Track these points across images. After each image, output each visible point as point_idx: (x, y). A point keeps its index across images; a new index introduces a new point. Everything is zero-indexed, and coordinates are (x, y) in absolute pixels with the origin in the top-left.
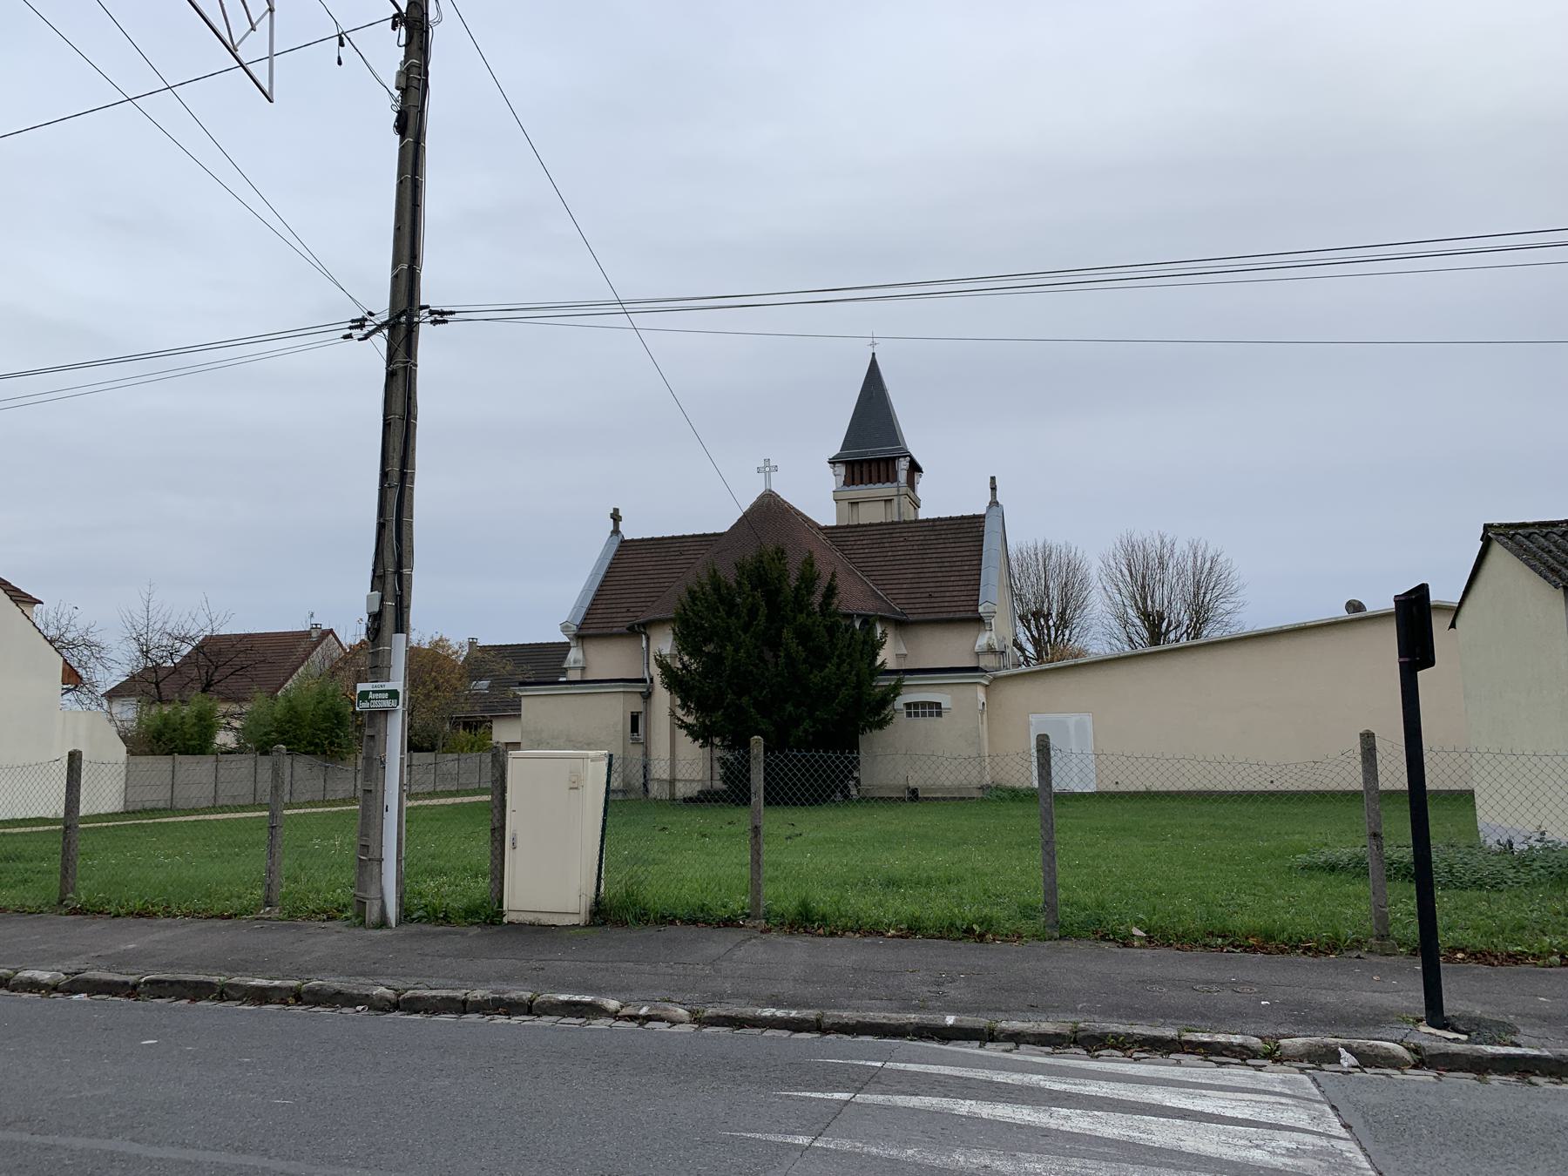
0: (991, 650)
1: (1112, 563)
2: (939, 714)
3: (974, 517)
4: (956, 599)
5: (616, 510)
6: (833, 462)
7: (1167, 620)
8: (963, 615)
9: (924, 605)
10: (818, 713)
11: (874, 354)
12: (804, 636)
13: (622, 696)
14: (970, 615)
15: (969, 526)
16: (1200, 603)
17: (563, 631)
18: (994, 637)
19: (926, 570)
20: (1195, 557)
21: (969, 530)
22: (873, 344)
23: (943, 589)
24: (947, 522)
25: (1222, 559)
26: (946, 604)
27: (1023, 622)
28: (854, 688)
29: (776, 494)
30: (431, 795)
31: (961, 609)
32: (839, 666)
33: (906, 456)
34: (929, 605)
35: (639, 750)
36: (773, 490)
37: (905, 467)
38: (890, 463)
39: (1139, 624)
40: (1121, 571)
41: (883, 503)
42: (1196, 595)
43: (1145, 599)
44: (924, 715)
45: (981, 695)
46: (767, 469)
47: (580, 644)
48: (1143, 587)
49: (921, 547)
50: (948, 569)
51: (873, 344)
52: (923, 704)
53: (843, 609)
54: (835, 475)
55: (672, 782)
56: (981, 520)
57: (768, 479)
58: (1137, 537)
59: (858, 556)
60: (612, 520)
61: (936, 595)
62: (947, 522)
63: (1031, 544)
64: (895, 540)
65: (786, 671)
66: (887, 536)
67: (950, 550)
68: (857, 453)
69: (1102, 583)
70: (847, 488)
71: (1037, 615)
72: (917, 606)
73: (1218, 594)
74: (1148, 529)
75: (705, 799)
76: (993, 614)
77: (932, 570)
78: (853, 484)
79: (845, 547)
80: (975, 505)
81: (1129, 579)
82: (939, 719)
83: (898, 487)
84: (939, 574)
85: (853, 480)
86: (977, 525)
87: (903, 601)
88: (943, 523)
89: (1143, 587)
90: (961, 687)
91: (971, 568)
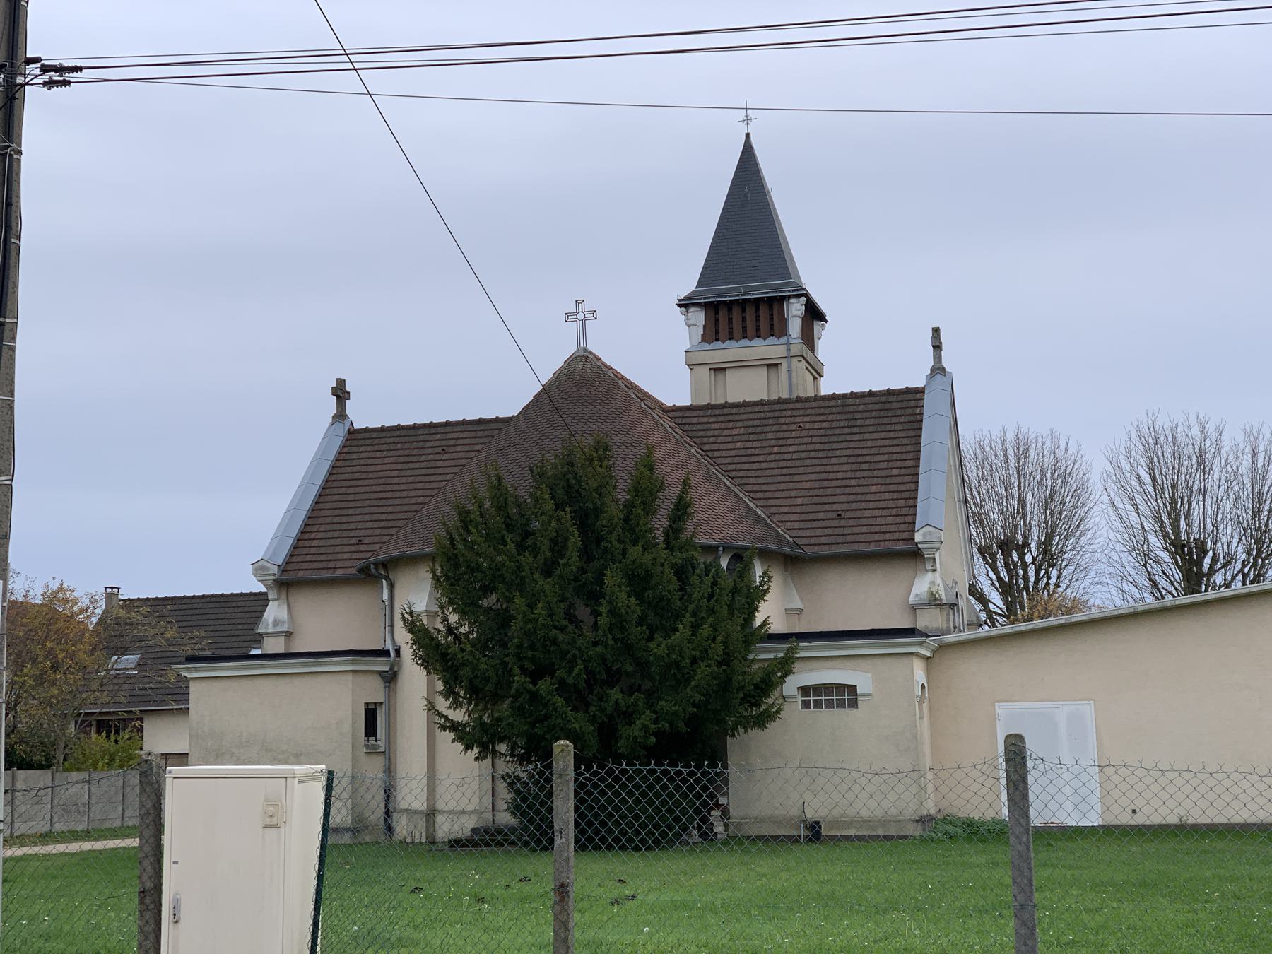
0: (934, 602)
2: (854, 704)
3: (908, 391)
4: (879, 521)
5: (341, 383)
6: (684, 304)
7: (1211, 553)
8: (890, 546)
11: (748, 135)
12: (639, 581)
13: (350, 677)
14: (900, 546)
17: (255, 575)
18: (939, 581)
19: (832, 476)
20: (1255, 455)
22: (747, 120)
24: (867, 400)
29: (595, 356)
31: (888, 536)
32: (695, 628)
36: (590, 348)
40: (1138, 477)
41: (766, 366)
44: (830, 705)
45: (919, 673)
46: (581, 316)
47: (284, 596)
48: (1173, 502)
50: (866, 474)
51: (747, 120)
52: (829, 688)
53: (702, 539)
55: (431, 814)
56: (918, 396)
57: (581, 333)
58: (1163, 423)
61: (849, 514)
63: (996, 434)
64: (784, 427)
65: (609, 636)
66: (771, 421)
67: (869, 443)
68: (723, 291)
69: (1109, 496)
71: (1006, 545)
72: (819, 532)
76: (937, 545)
79: (705, 440)
81: (1151, 489)
83: (788, 344)
84: (853, 482)
85: (717, 333)
86: (912, 404)
87: (796, 525)
88: (858, 401)
89: (1173, 502)
91: (903, 471)
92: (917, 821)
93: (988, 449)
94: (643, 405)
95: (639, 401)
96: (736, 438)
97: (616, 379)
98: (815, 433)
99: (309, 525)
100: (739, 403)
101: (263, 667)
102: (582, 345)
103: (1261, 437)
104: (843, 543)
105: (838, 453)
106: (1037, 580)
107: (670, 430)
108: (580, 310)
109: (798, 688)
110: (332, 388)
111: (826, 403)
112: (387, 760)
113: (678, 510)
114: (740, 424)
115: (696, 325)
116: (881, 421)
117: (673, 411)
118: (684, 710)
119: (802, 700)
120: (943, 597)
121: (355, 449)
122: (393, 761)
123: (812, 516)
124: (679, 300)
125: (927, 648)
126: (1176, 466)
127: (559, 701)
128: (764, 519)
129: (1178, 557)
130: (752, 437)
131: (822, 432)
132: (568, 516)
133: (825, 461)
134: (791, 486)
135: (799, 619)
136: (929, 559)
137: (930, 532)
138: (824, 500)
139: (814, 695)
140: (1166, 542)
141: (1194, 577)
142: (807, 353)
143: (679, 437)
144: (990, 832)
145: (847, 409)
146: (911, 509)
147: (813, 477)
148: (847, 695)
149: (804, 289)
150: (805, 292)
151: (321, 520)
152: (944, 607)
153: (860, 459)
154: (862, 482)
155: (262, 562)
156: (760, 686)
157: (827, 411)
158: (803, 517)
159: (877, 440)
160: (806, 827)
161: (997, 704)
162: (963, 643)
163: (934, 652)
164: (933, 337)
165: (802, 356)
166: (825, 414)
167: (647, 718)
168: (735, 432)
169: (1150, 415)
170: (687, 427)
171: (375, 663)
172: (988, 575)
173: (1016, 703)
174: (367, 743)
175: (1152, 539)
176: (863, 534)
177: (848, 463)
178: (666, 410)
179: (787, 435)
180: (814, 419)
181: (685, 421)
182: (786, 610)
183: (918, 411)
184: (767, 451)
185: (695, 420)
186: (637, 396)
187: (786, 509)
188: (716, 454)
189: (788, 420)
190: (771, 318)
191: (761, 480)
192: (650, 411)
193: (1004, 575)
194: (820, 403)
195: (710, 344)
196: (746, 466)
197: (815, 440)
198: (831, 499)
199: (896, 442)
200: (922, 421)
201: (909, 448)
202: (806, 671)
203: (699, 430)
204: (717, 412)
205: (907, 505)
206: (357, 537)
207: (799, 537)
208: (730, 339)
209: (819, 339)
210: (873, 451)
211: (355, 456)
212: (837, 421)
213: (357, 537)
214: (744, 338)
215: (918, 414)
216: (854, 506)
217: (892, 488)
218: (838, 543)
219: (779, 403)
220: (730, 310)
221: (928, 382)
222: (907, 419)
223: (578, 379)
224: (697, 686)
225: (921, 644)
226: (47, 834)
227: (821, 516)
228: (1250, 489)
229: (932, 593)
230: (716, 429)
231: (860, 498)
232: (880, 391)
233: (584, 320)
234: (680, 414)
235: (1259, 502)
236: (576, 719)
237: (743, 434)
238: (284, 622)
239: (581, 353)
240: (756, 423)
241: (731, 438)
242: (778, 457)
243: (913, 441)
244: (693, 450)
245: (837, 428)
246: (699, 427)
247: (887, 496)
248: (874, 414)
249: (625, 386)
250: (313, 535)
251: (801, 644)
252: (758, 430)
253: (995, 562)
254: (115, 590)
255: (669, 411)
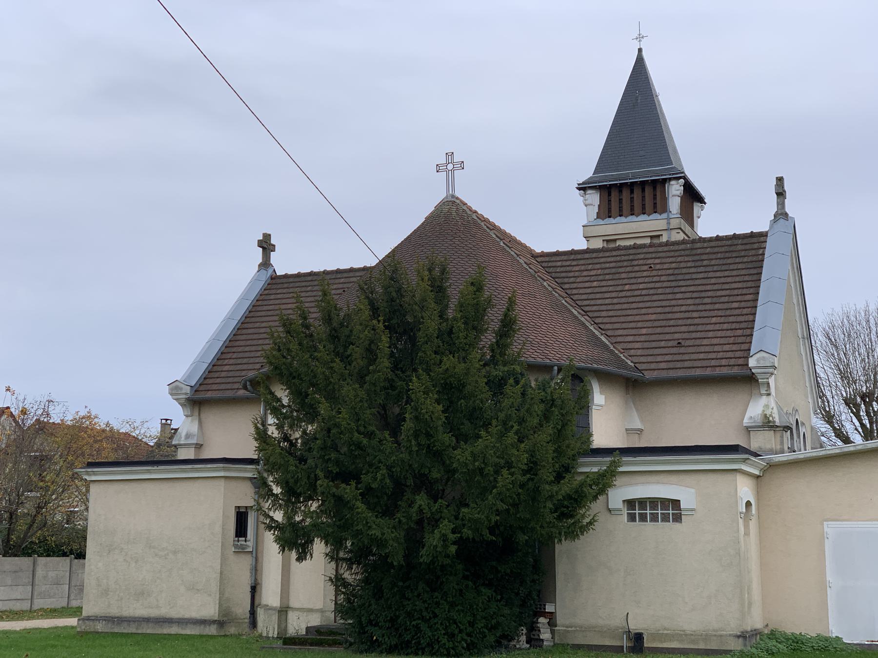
0: (768, 424)
2: (678, 518)
3: (752, 235)
4: (716, 348)
5: (267, 237)
6: (583, 188)
8: (725, 371)
11: (640, 50)
13: (222, 482)
14: (736, 371)
17: (171, 394)
18: (773, 404)
19: (676, 309)
21: (743, 253)
22: (640, 38)
23: (698, 335)
24: (713, 244)
26: (702, 356)
27: (850, 408)
28: (525, 472)
29: (462, 202)
31: (724, 362)
32: (502, 435)
33: (680, 178)
36: (457, 194)
41: (650, 238)
44: (654, 518)
45: (745, 490)
46: (450, 167)
47: (196, 417)
49: (672, 278)
50: (708, 307)
51: (640, 38)
52: (654, 502)
53: (533, 356)
55: (283, 611)
56: (762, 239)
57: (450, 182)
62: (713, 244)
63: (861, 306)
64: (637, 268)
66: (625, 264)
67: (713, 281)
68: (614, 176)
70: (600, 222)
72: (659, 359)
76: (771, 370)
79: (566, 280)
82: (677, 525)
83: (668, 219)
84: (695, 315)
85: (610, 211)
86: (756, 246)
87: (639, 352)
91: (743, 304)
92: (739, 637)
93: (853, 319)
94: (502, 244)
95: (498, 240)
96: (593, 278)
97: (479, 221)
98: (663, 272)
99: (225, 353)
100: (599, 248)
101: (149, 472)
102: (451, 192)
104: (680, 368)
105: (683, 289)
107: (525, 266)
108: (450, 162)
109: (624, 501)
110: (258, 241)
111: (676, 247)
112: (254, 559)
113: (504, 326)
114: (598, 266)
115: (592, 205)
116: (725, 261)
117: (541, 256)
118: (487, 517)
119: (628, 513)
120: (777, 420)
121: (274, 291)
122: (260, 559)
123: (654, 344)
124: (579, 184)
127: (360, 506)
128: (607, 346)
130: (607, 277)
131: (670, 272)
132: (381, 325)
133: (670, 297)
134: (637, 318)
136: (763, 383)
137: (764, 357)
138: (667, 330)
142: (685, 226)
144: (814, 649)
145: (694, 252)
146: (748, 338)
147: (659, 310)
150: (683, 175)
152: (777, 429)
153: (703, 294)
155: (177, 383)
156: (573, 496)
157: (677, 254)
158: (646, 345)
159: (720, 277)
160: (629, 639)
162: (792, 463)
164: (777, 185)
165: (680, 228)
166: (675, 257)
171: (246, 471)
172: (852, 421)
173: (844, 523)
174: (236, 543)
176: (700, 360)
177: (692, 298)
178: (535, 256)
179: (639, 274)
180: (664, 260)
181: (550, 264)
183: (761, 252)
184: (619, 288)
185: (559, 264)
186: (497, 236)
187: (630, 339)
188: (575, 291)
189: (641, 262)
192: (508, 249)
194: (671, 247)
195: (603, 220)
196: (599, 302)
197: (663, 278)
198: (673, 330)
199: (737, 279)
200: (763, 261)
201: (749, 284)
202: (631, 485)
203: (562, 272)
204: (579, 257)
205: (744, 334)
206: (260, 363)
207: (640, 363)
208: (621, 216)
210: (716, 287)
211: (272, 297)
212: (685, 262)
213: (260, 363)
214: (631, 215)
215: (761, 255)
216: (694, 335)
217: (731, 319)
218: (677, 369)
219: (634, 248)
220: (621, 192)
221: (771, 227)
222: (750, 259)
223: (443, 220)
224: (500, 494)
225: (744, 461)
227: (663, 344)
229: (765, 415)
230: (577, 271)
231: (700, 328)
232: (726, 236)
233: (453, 170)
234: (547, 259)
236: (378, 526)
237: (600, 275)
238: (194, 435)
239: (450, 199)
240: (612, 265)
241: (589, 278)
242: (628, 294)
243: (755, 278)
244: (545, 284)
245: (684, 268)
247: (725, 326)
248: (719, 256)
249: (488, 227)
250: (226, 362)
251: (624, 459)
252: (613, 271)
253: (858, 411)
254: (169, 422)
255: (537, 257)
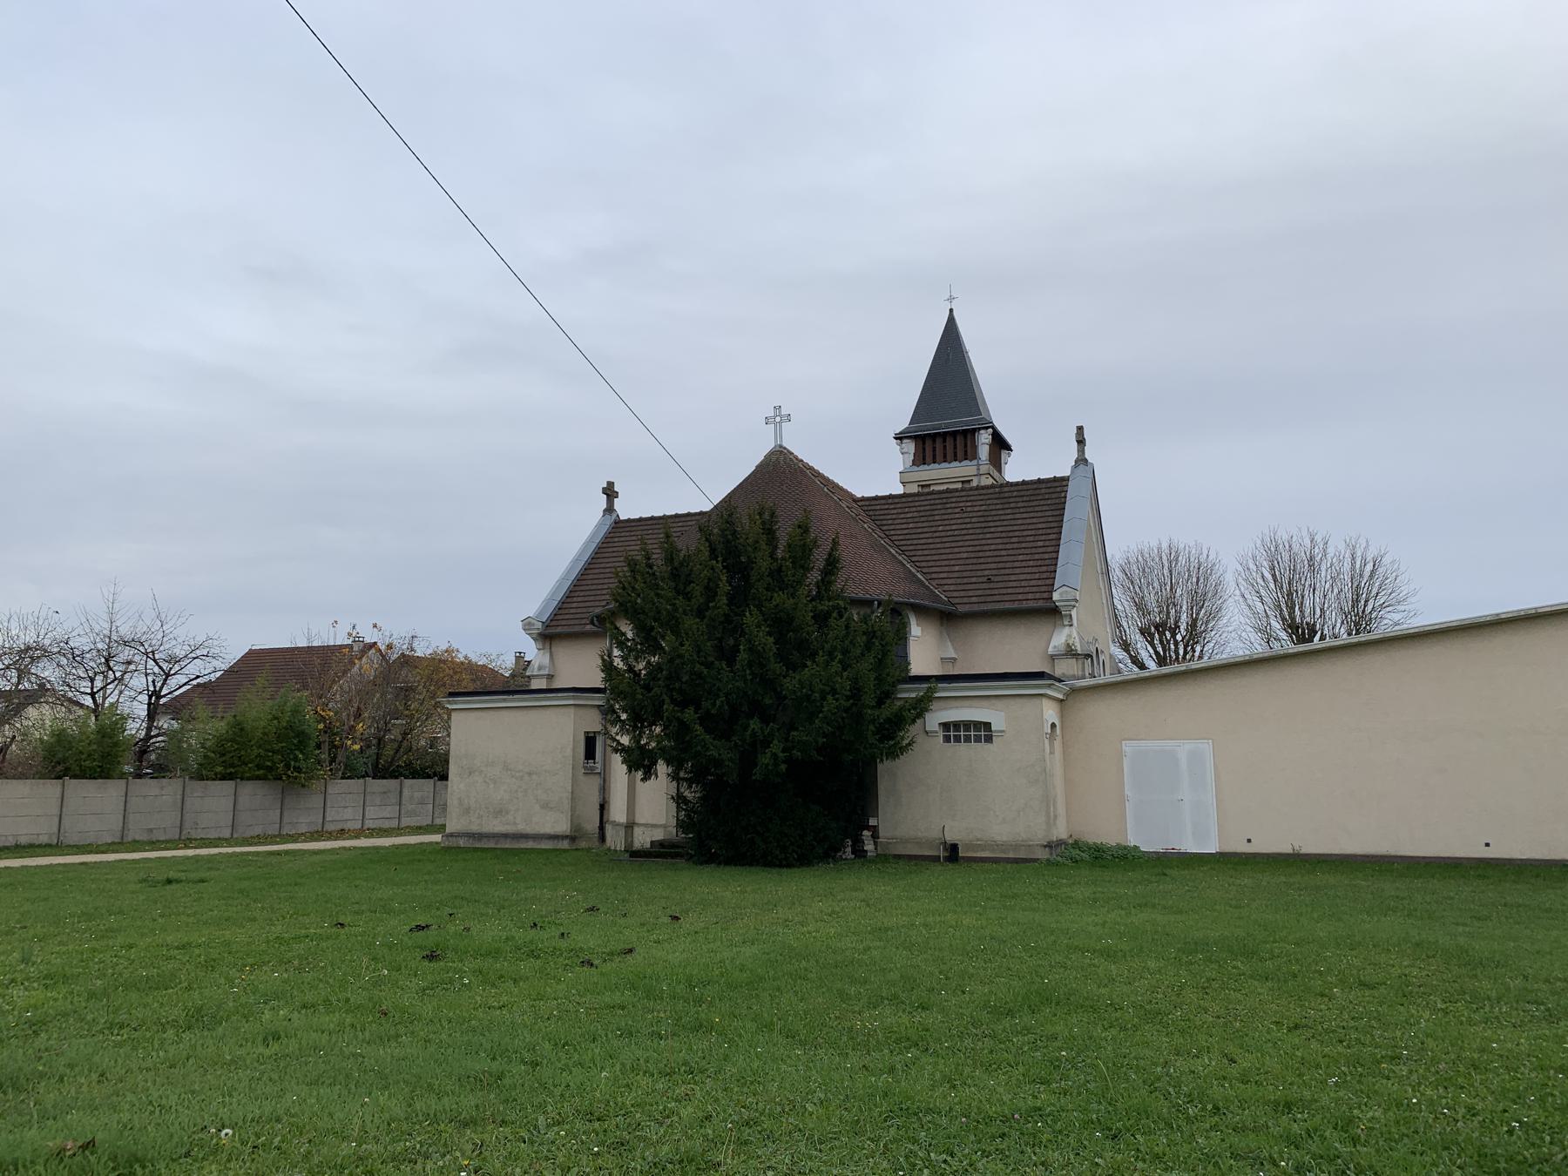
0: (1070, 653)
1: (1252, 567)
2: (989, 739)
3: (1055, 479)
5: (611, 484)
6: (900, 438)
7: (1319, 633)
8: (1032, 604)
9: (979, 593)
10: (795, 733)
11: (951, 310)
12: (781, 624)
13: (572, 710)
14: (1041, 604)
15: (1047, 491)
16: (1360, 611)
18: (1075, 634)
19: (986, 548)
20: (1353, 559)
22: (951, 299)
25: (1386, 560)
28: (848, 698)
29: (788, 451)
30: (398, 831)
31: (1030, 596)
34: (988, 592)
35: (595, 782)
36: (784, 445)
37: (987, 441)
38: (969, 436)
39: (1285, 638)
40: (1263, 576)
42: (1356, 602)
43: (1291, 609)
44: (968, 739)
45: (1050, 713)
46: (778, 419)
47: (547, 646)
48: (1290, 594)
50: (1015, 546)
51: (951, 299)
52: (967, 725)
53: (855, 592)
54: (902, 454)
55: (630, 827)
56: (1064, 483)
57: (778, 433)
58: (1283, 536)
59: (899, 532)
60: (605, 496)
61: (997, 579)
63: (1154, 544)
64: (950, 511)
65: (748, 672)
66: (939, 507)
67: (1020, 522)
68: (929, 426)
69: (1240, 590)
70: (916, 468)
71: (1161, 627)
73: (1382, 602)
74: (1294, 530)
75: (662, 852)
76: (1073, 603)
77: (993, 547)
78: (924, 464)
79: (885, 522)
80: (1056, 463)
81: (1272, 586)
84: (1003, 553)
85: (924, 459)
86: (1058, 489)
87: (952, 588)
88: (1012, 489)
89: (1290, 594)
90: (1019, 701)
91: (1047, 543)
92: (1045, 846)
94: (826, 489)
97: (805, 469)
103: (1358, 546)
105: (992, 530)
106: (1186, 653)
107: (847, 509)
109: (940, 724)
120: (1079, 648)
125: (1060, 692)
126: (1292, 568)
129: (1294, 637)
130: (923, 519)
135: (953, 666)
136: (1066, 615)
139: (956, 731)
140: (1284, 624)
141: (1301, 632)
143: (854, 516)
145: (1002, 495)
147: (970, 549)
148: (982, 732)
149: (991, 423)
151: (582, 588)
153: (1011, 534)
154: (1010, 552)
157: (986, 497)
161: (1123, 742)
163: (1067, 695)
167: (776, 747)
168: (909, 515)
169: (1272, 529)
170: (871, 513)
171: (593, 699)
175: (1274, 623)
178: (856, 500)
181: (870, 508)
182: (942, 659)
183: (1063, 495)
184: (933, 529)
185: (878, 507)
189: (953, 505)
190: (966, 446)
191: (926, 552)
192: (831, 494)
193: (1160, 649)
199: (1042, 520)
202: (945, 709)
204: (896, 501)
208: (934, 463)
209: (1006, 463)
210: (1022, 527)
211: (616, 540)
216: (1003, 572)
217: (1037, 557)
221: (1072, 472)
225: (1049, 686)
226: (279, 835)
228: (1350, 585)
229: (1068, 644)
234: (867, 503)
235: (1357, 595)
236: (715, 747)
239: (778, 449)
242: (943, 534)
246: (882, 512)
247: (1031, 563)
248: (1025, 499)
251: (940, 685)
253: (1153, 639)
254: (522, 655)
